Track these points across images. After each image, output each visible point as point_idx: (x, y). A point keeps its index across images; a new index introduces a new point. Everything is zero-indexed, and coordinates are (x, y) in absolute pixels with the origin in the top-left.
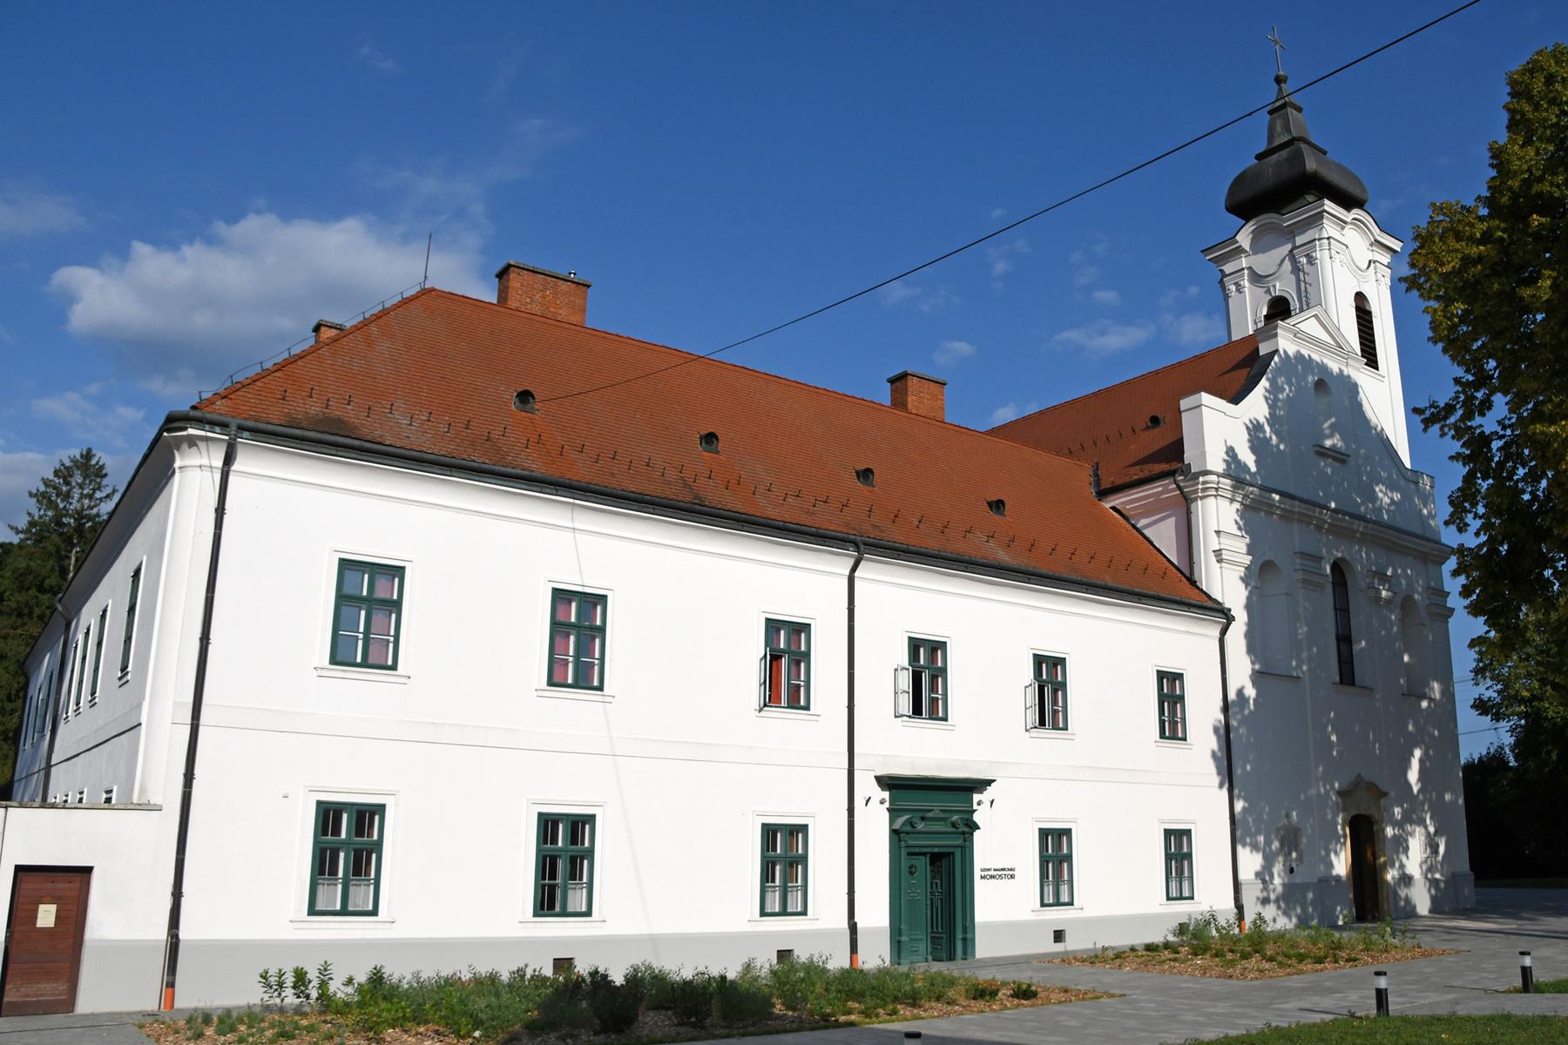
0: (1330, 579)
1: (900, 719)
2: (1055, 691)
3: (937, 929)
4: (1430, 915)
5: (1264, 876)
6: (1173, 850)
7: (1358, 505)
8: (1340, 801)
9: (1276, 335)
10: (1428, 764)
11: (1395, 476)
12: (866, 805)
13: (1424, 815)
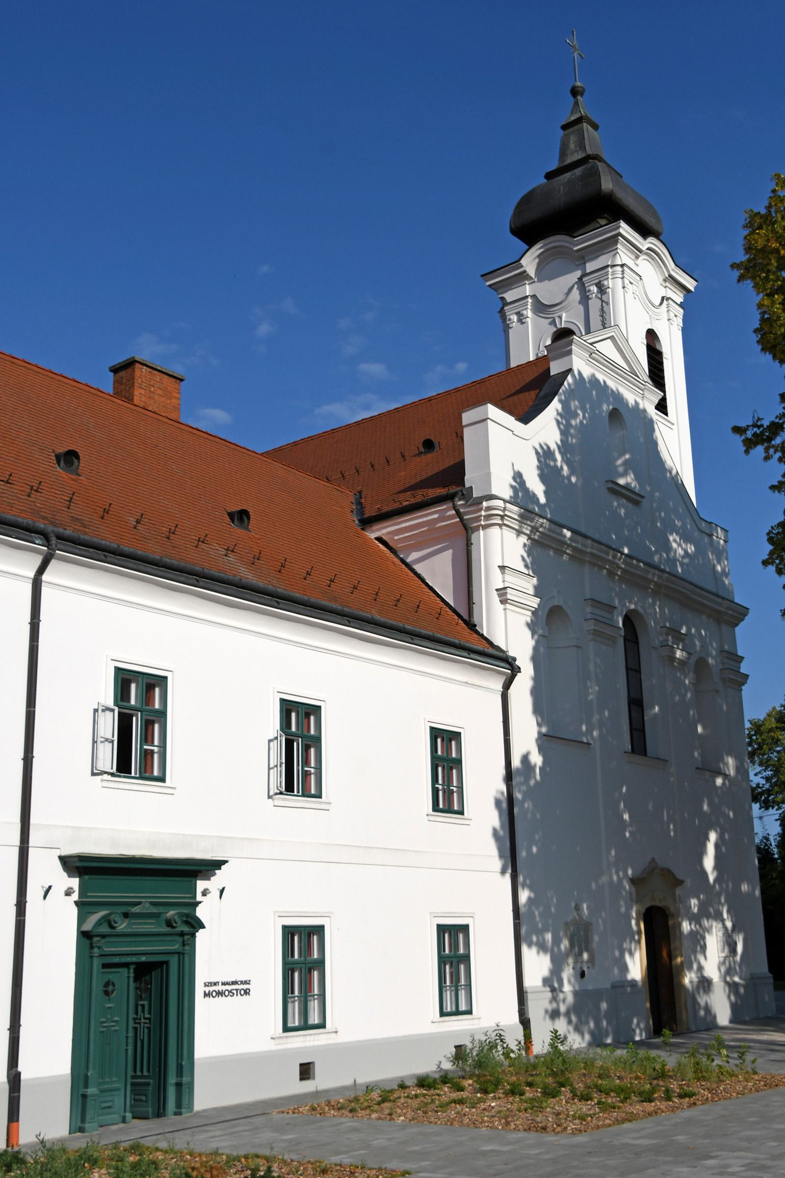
0: (622, 633)
1: (100, 777)
2: (307, 748)
3: (142, 1071)
4: (731, 1025)
5: (552, 983)
6: (447, 951)
7: (652, 554)
8: (633, 890)
9: (570, 352)
10: (723, 849)
11: (689, 526)
12: (45, 897)
13: (721, 907)
